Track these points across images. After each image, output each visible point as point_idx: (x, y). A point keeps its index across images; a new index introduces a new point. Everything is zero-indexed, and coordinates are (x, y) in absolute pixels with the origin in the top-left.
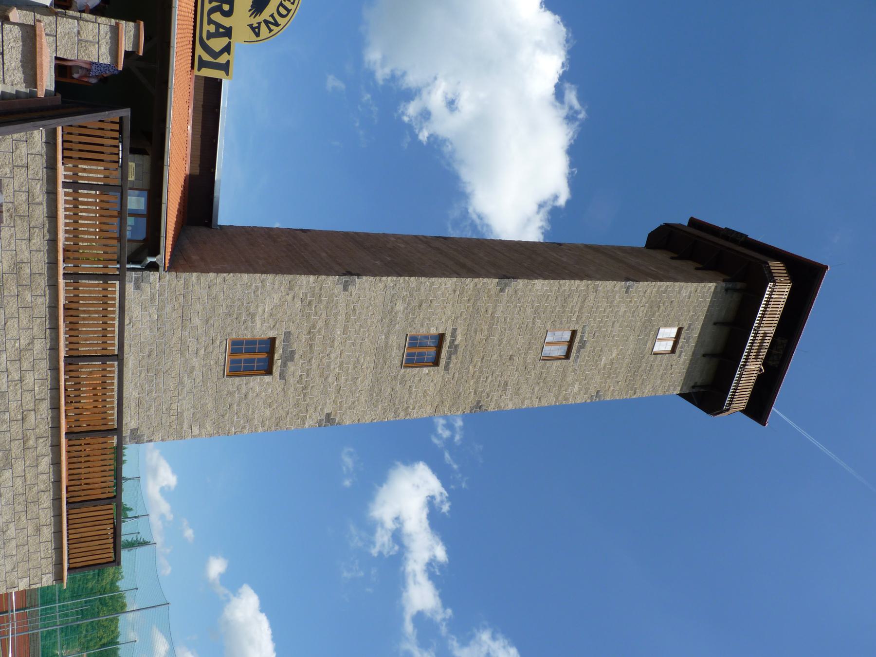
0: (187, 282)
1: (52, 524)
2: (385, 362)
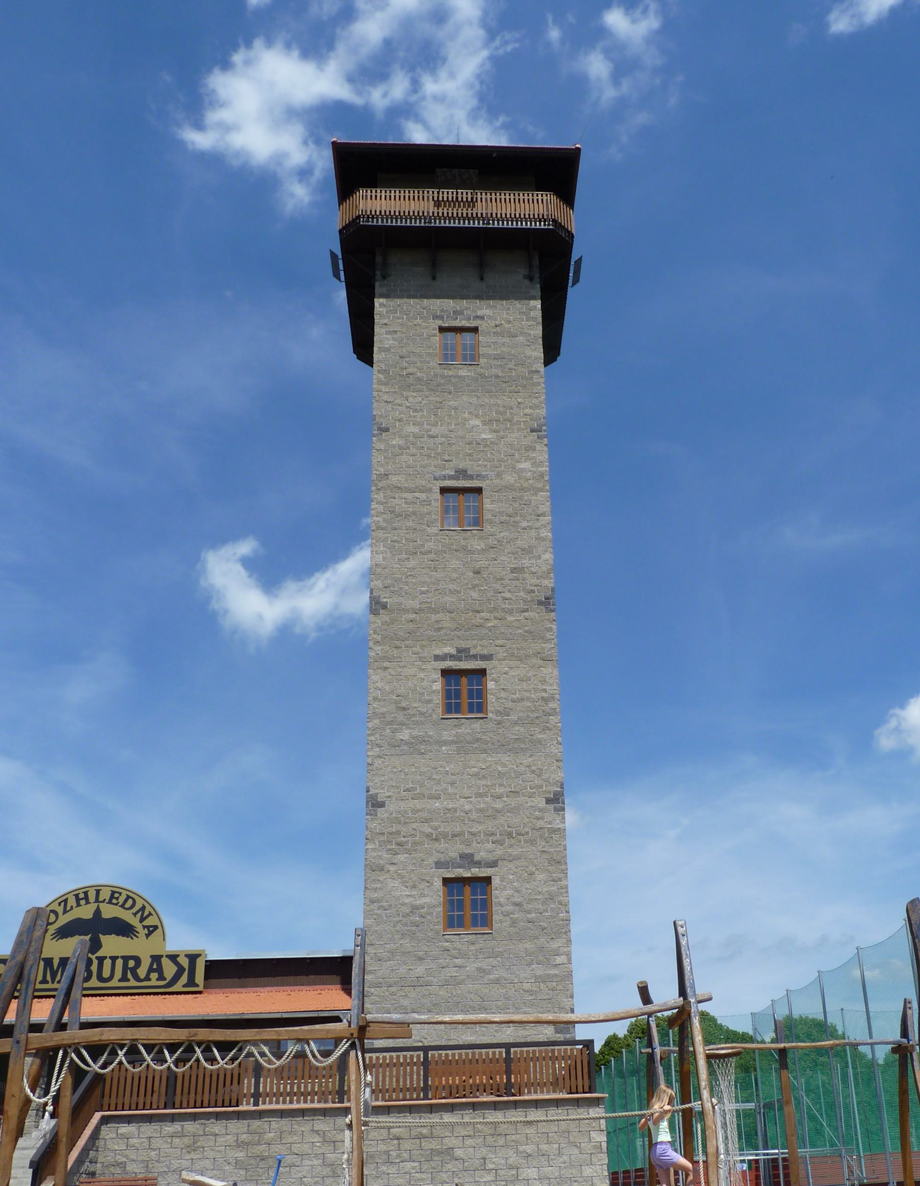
0: (374, 984)
1: (525, 1110)
2: (478, 740)
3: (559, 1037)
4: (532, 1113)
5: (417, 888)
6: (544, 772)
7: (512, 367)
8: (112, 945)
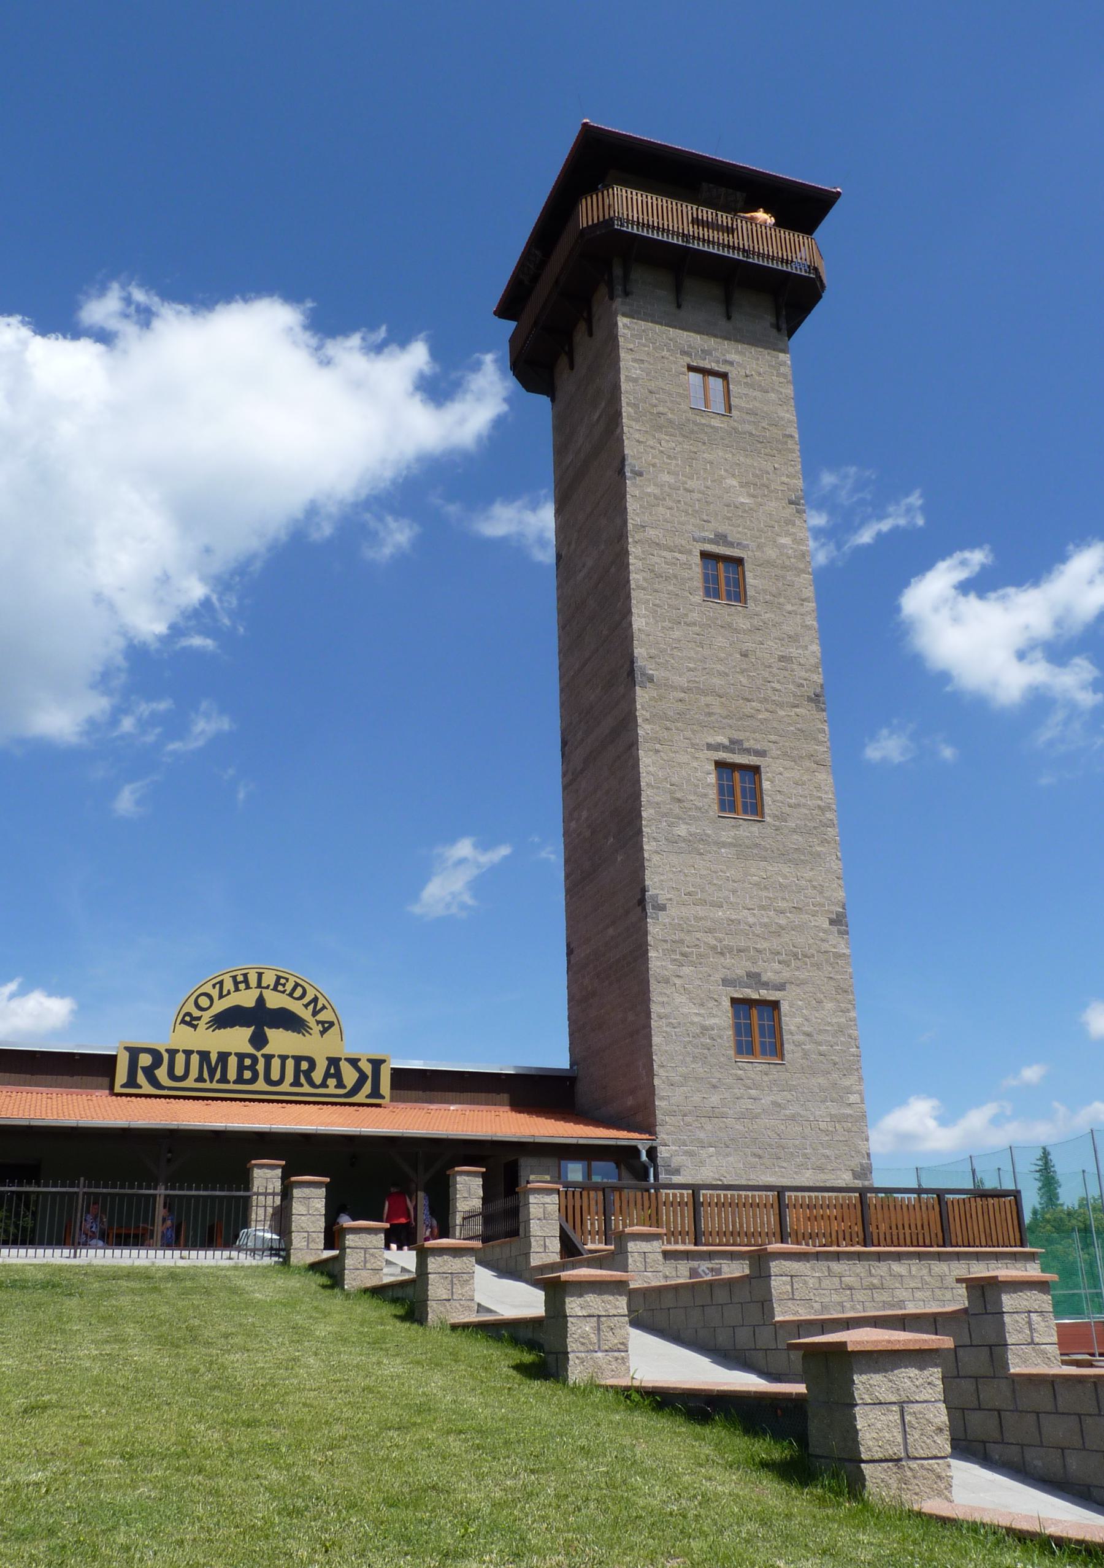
2: (757, 845)
3: (858, 1184)
4: (974, 1266)
5: (706, 1007)
6: (825, 889)
7: (766, 427)
8: (280, 1041)
